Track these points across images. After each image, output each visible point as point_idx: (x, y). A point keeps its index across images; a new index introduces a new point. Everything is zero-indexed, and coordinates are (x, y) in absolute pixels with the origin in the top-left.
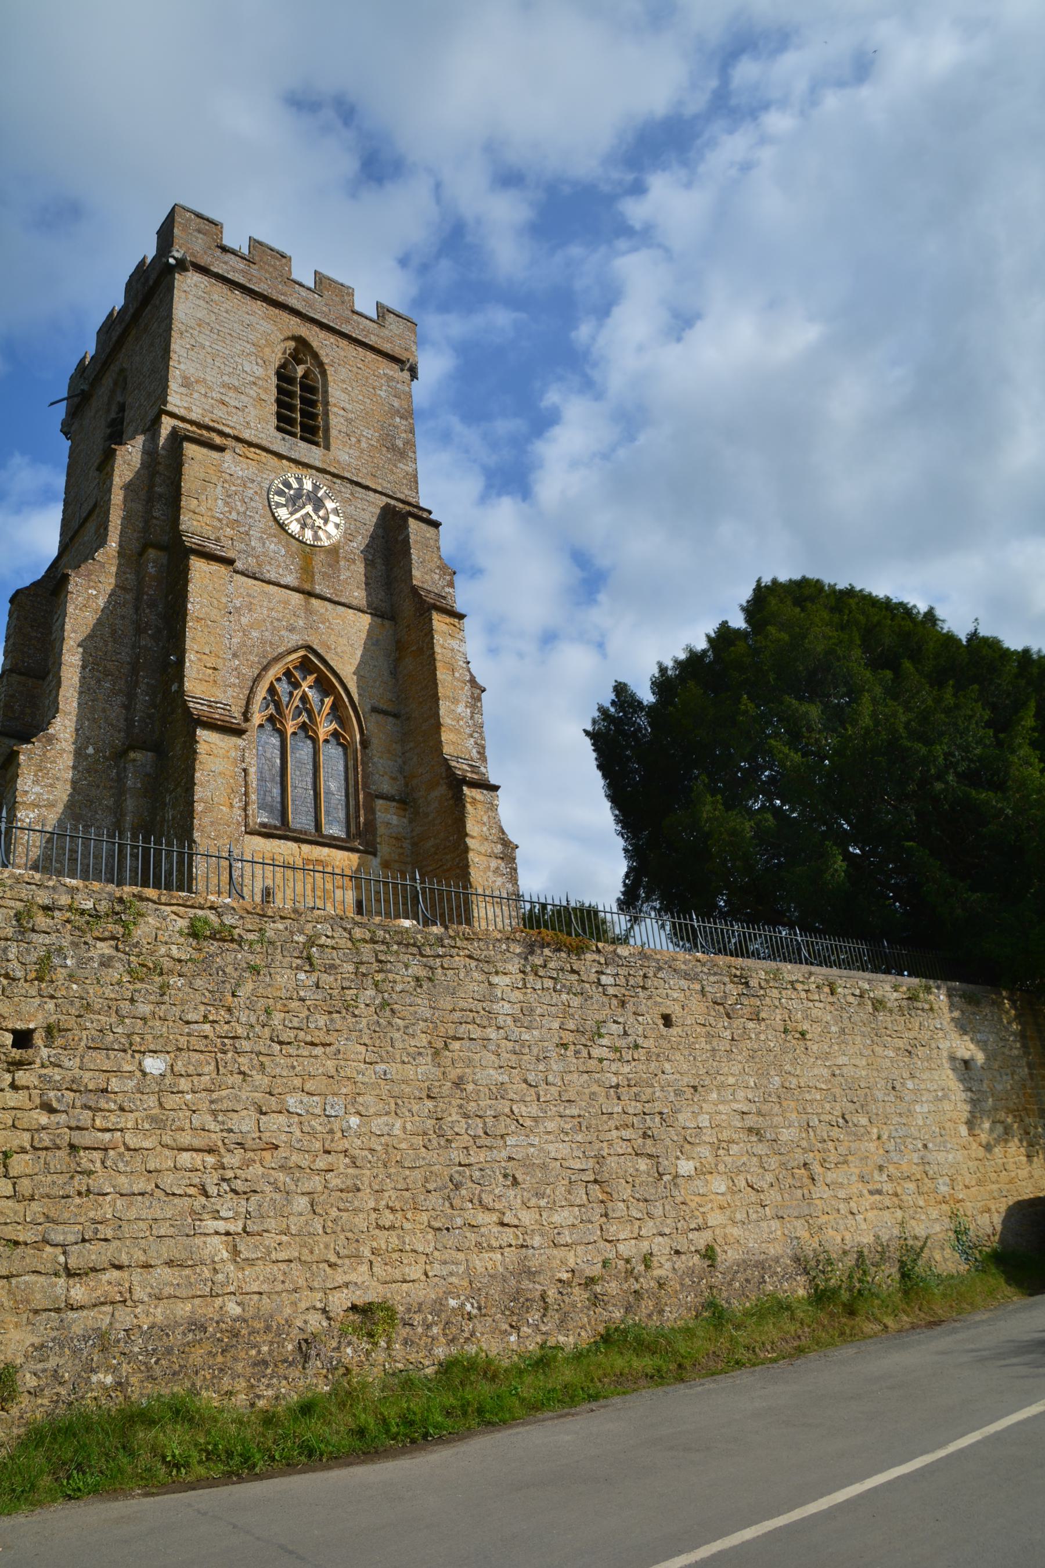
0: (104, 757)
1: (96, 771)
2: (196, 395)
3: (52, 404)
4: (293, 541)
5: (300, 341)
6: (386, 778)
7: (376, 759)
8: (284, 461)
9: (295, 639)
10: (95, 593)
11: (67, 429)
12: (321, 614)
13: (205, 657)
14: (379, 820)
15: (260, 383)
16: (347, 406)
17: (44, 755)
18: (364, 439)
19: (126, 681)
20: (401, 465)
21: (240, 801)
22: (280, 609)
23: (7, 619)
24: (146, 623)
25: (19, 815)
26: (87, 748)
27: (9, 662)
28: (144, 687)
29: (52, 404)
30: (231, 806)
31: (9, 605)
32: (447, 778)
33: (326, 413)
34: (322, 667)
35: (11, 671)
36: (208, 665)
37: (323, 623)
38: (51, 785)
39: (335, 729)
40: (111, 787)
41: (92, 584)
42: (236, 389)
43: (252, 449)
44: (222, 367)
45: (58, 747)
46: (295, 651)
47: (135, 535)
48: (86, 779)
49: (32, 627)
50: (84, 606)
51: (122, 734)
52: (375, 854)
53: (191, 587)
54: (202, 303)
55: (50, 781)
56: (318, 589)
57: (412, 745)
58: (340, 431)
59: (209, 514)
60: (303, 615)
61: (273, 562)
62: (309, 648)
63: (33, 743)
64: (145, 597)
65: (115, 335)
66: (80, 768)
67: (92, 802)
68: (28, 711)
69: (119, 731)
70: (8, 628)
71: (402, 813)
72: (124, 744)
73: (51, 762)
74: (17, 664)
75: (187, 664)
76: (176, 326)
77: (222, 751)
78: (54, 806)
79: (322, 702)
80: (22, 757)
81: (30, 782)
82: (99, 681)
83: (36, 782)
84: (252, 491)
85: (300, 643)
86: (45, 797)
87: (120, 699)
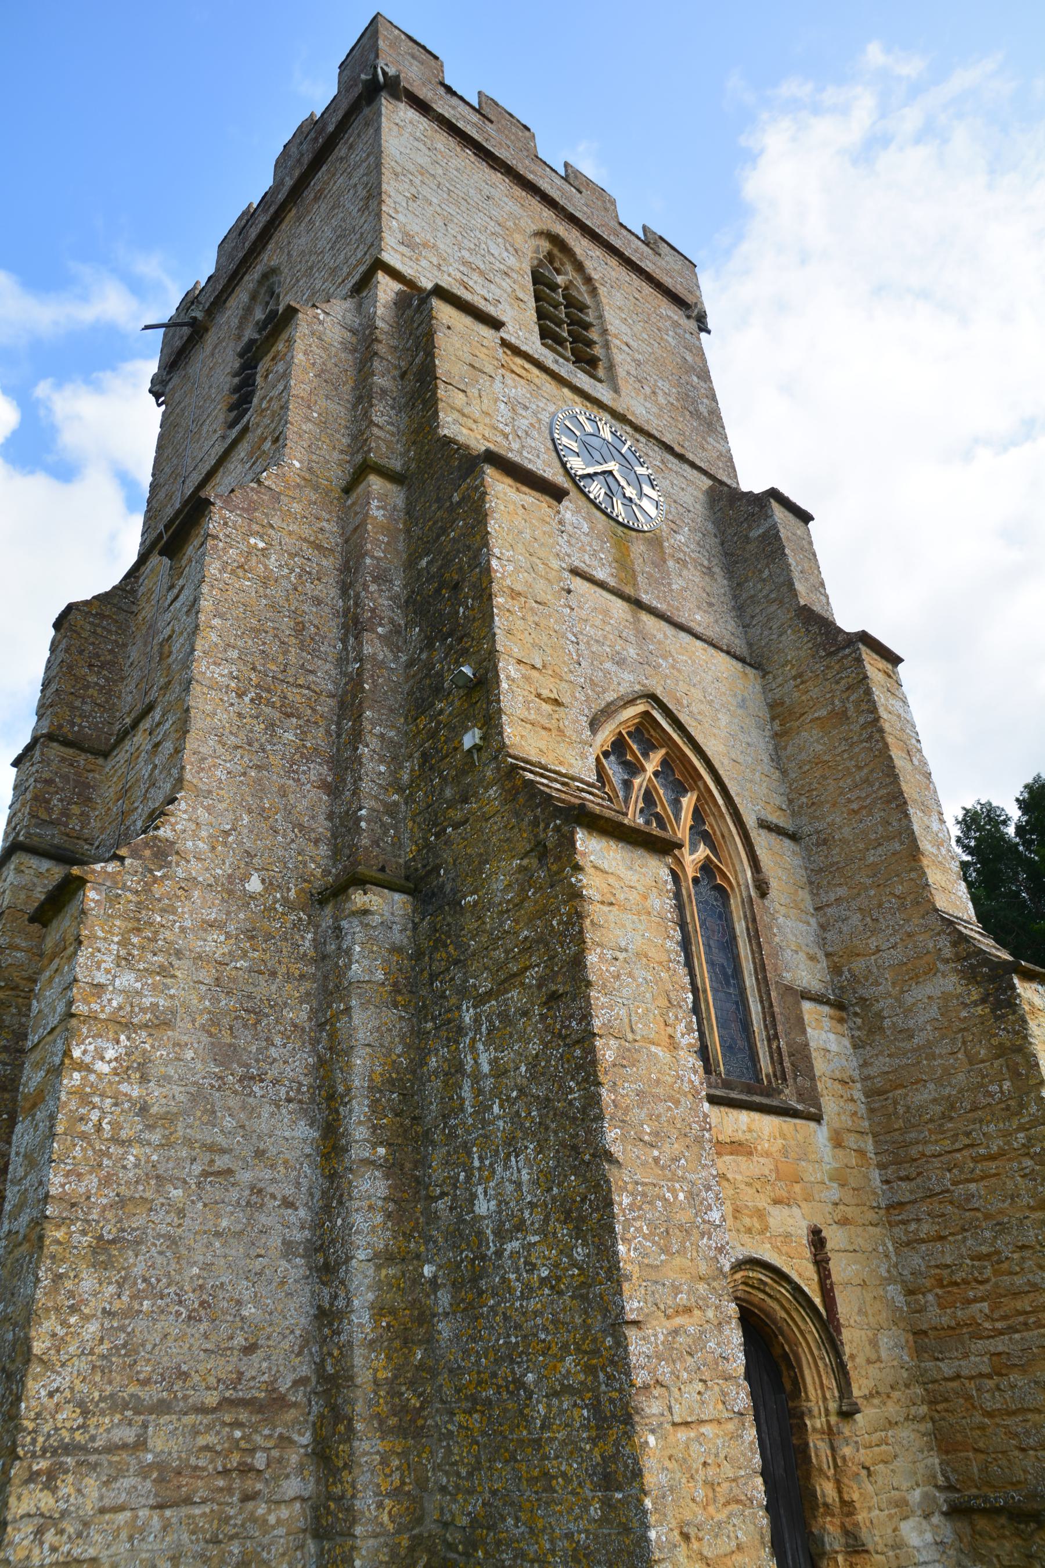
0: (285, 901)
1: (269, 937)
2: (424, 263)
3: (147, 327)
4: (598, 514)
5: (555, 240)
6: (802, 956)
7: (781, 920)
8: (566, 391)
9: (627, 682)
10: (261, 545)
11: (158, 389)
12: (660, 643)
13: (535, 674)
14: (813, 1045)
15: (514, 275)
16: (631, 343)
17: (147, 890)
18: (660, 393)
19: (328, 732)
20: (710, 440)
21: (689, 1030)
22: (598, 623)
23: (48, 654)
24: (373, 611)
25: (77, 1053)
26: (246, 878)
27: (46, 723)
28: (374, 743)
29: (147, 327)
30: (673, 1045)
31: (52, 632)
32: (959, 959)
33: (607, 345)
34: (675, 736)
35: (50, 737)
36: (545, 693)
37: (664, 658)
38: (163, 971)
39: (708, 857)
40: (302, 976)
41: (255, 527)
42: (482, 273)
43: (519, 361)
44: (459, 237)
45: (180, 873)
46: (631, 702)
47: (336, 455)
48: (245, 955)
49: (91, 666)
50: (241, 567)
51: (323, 850)
52: (817, 1119)
53: (492, 526)
54: (421, 146)
55: (159, 959)
56: (645, 598)
57: (842, 892)
58: (628, 373)
59: (487, 420)
60: (632, 639)
61: (573, 541)
62: (653, 698)
63: (121, 859)
64: (368, 561)
65: (253, 233)
66: (231, 928)
67: (258, 1013)
68: (75, 810)
69: (316, 842)
70: (48, 668)
71: (840, 1028)
72: (326, 873)
73: (163, 911)
74: (60, 727)
75: (504, 685)
76: (388, 164)
77: (634, 896)
78: (167, 1024)
79: (676, 804)
80: (92, 894)
81: (109, 962)
82: (271, 726)
83: (125, 961)
84: (526, 422)
85: (637, 688)
86: (147, 1002)
87: (318, 771)
